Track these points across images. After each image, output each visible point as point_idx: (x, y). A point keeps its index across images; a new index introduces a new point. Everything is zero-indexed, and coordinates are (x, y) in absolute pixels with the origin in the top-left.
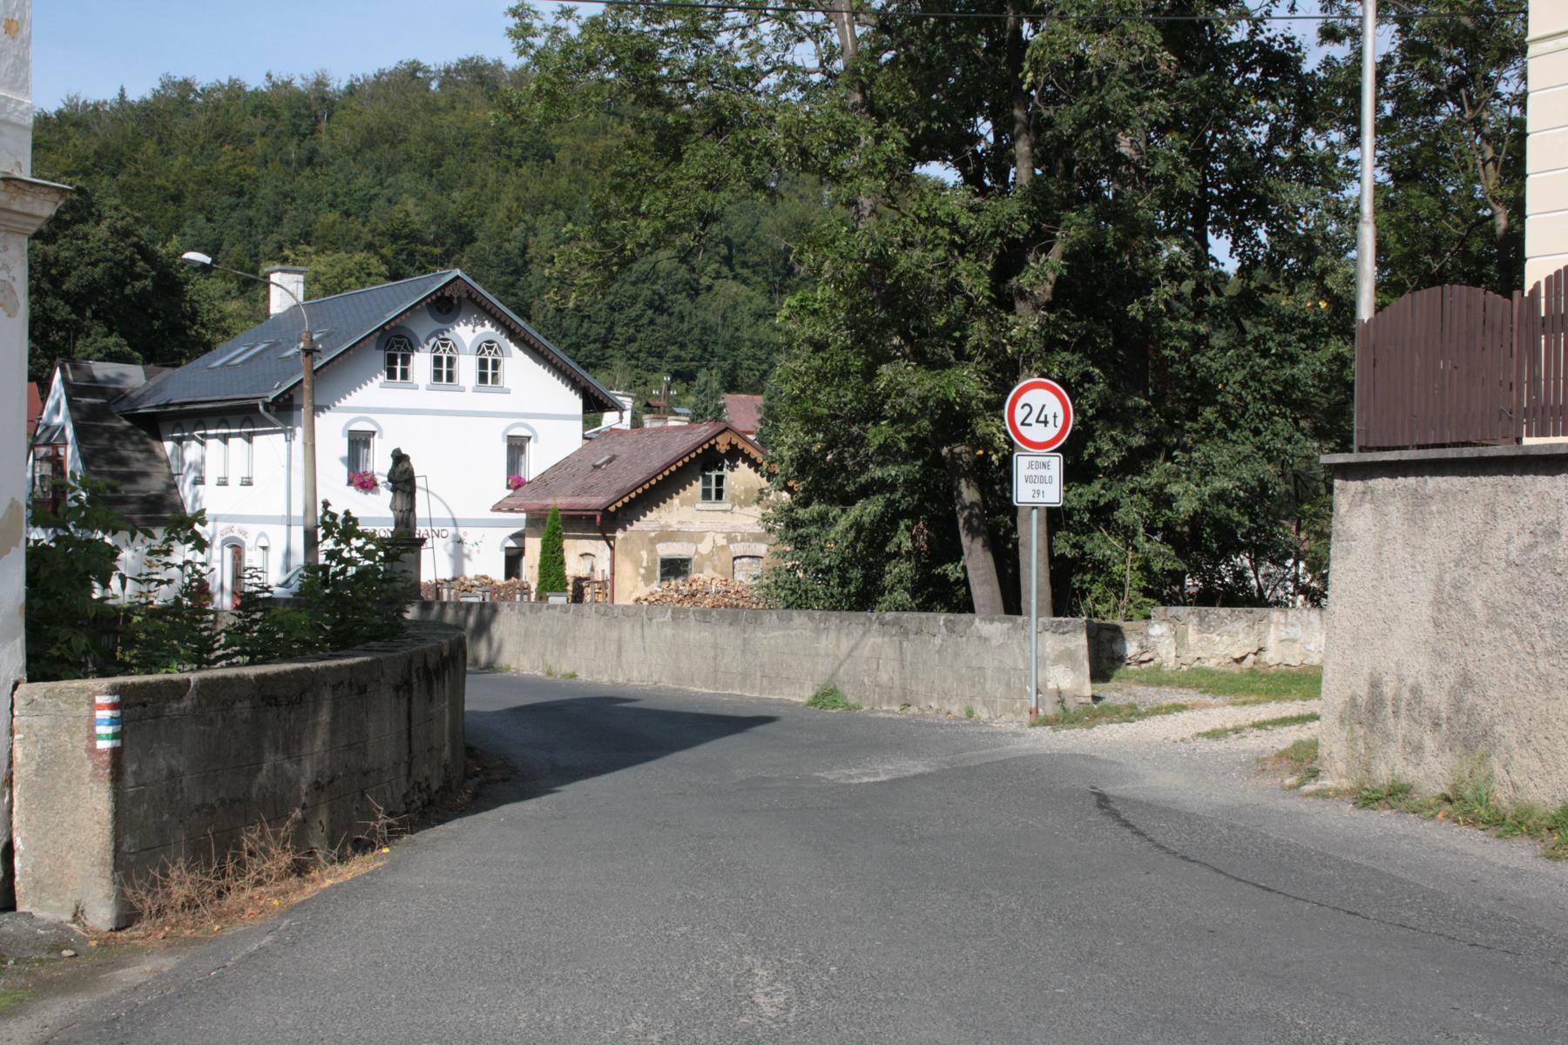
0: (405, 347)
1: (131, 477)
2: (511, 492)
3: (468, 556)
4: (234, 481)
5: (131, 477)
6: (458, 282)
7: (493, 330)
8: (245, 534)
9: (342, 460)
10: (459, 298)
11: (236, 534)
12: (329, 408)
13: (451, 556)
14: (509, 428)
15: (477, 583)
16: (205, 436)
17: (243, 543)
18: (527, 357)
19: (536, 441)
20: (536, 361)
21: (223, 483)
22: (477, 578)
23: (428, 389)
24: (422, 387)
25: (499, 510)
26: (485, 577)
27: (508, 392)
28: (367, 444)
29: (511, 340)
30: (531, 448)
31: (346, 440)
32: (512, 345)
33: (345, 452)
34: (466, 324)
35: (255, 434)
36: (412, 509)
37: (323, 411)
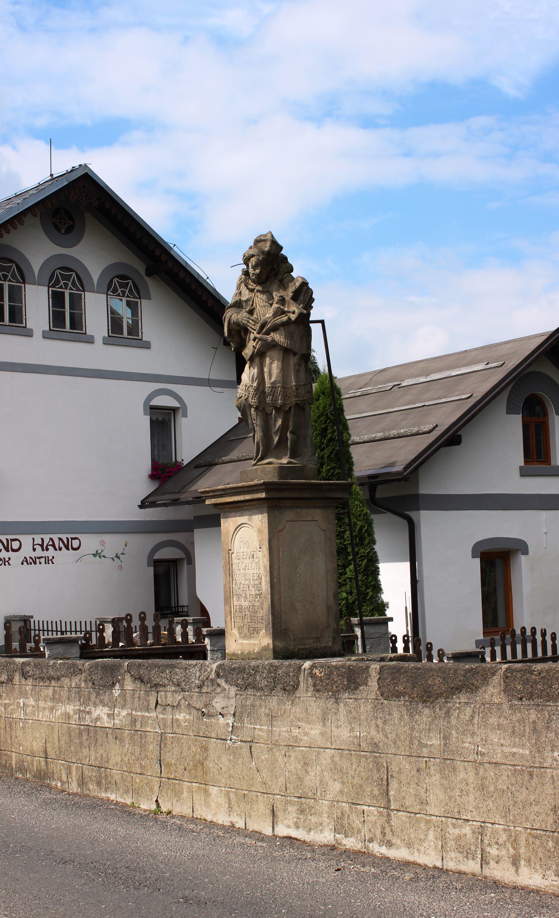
0: (13, 276)
23: (45, 336)
24: (38, 334)
25: (153, 505)
27: (147, 346)
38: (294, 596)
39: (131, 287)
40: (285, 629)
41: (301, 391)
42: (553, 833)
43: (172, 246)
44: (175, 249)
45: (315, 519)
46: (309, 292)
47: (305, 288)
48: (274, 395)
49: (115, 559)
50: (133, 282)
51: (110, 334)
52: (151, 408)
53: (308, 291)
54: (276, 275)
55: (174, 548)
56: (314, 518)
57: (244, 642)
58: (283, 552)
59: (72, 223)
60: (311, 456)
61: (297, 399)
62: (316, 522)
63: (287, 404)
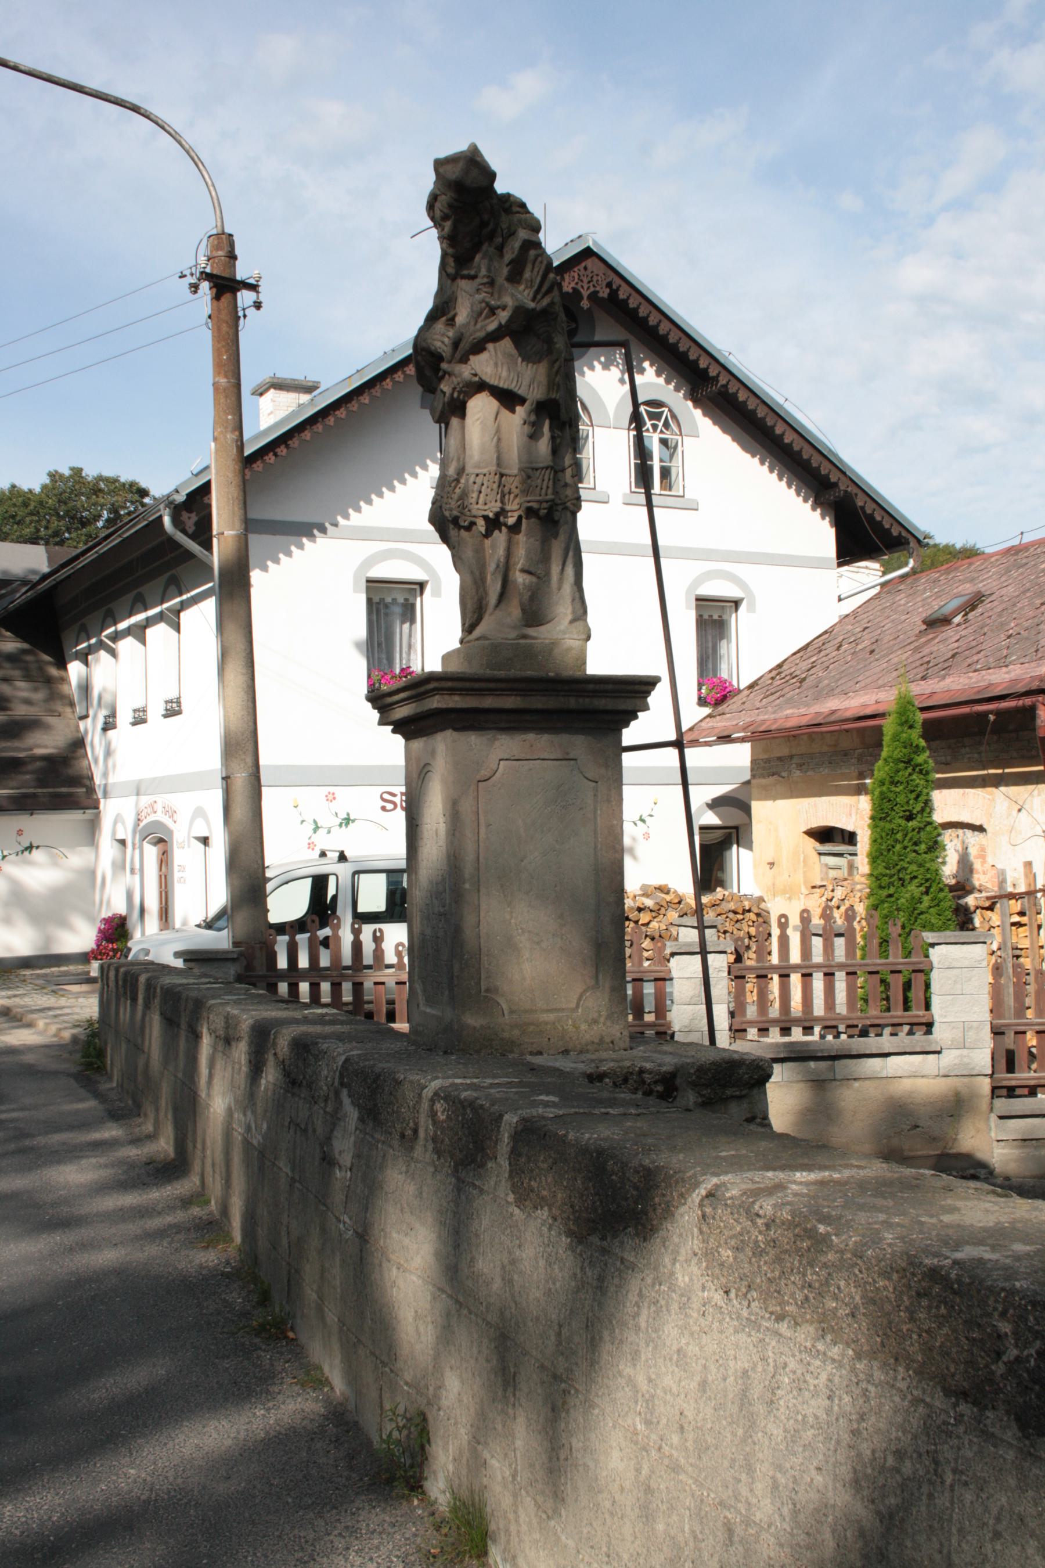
1: (17, 729)
2: (707, 711)
3: (631, 851)
4: (155, 712)
5: (17, 729)
6: (589, 263)
7: (661, 380)
8: (172, 813)
9: (358, 645)
10: (593, 297)
11: (160, 817)
12: (323, 530)
13: (32, 814)
14: (699, 581)
15: (649, 903)
16: (116, 637)
17: (170, 833)
18: (727, 438)
19: (752, 609)
20: (746, 448)
21: (139, 720)
22: (646, 892)
26: (664, 890)
27: (693, 507)
28: (409, 613)
29: (697, 402)
30: (741, 623)
31: (362, 598)
32: (698, 413)
33: (360, 630)
34: (606, 367)
35: (184, 606)
36: (123, 1145)
37: (311, 536)
38: (513, 921)
39: (666, 418)
40: (487, 990)
41: (539, 481)
42: (988, 1561)
43: (727, 354)
44: (731, 358)
45: (571, 756)
46: (541, 262)
47: (532, 253)
48: (480, 492)
49: (639, 823)
50: (670, 411)
51: (633, 489)
52: (697, 600)
53: (540, 259)
54: (491, 237)
55: (727, 808)
56: (567, 754)
57: (428, 1010)
58: (488, 825)
59: (574, 326)
60: (572, 622)
61: (529, 498)
62: (572, 762)
63: (512, 511)
